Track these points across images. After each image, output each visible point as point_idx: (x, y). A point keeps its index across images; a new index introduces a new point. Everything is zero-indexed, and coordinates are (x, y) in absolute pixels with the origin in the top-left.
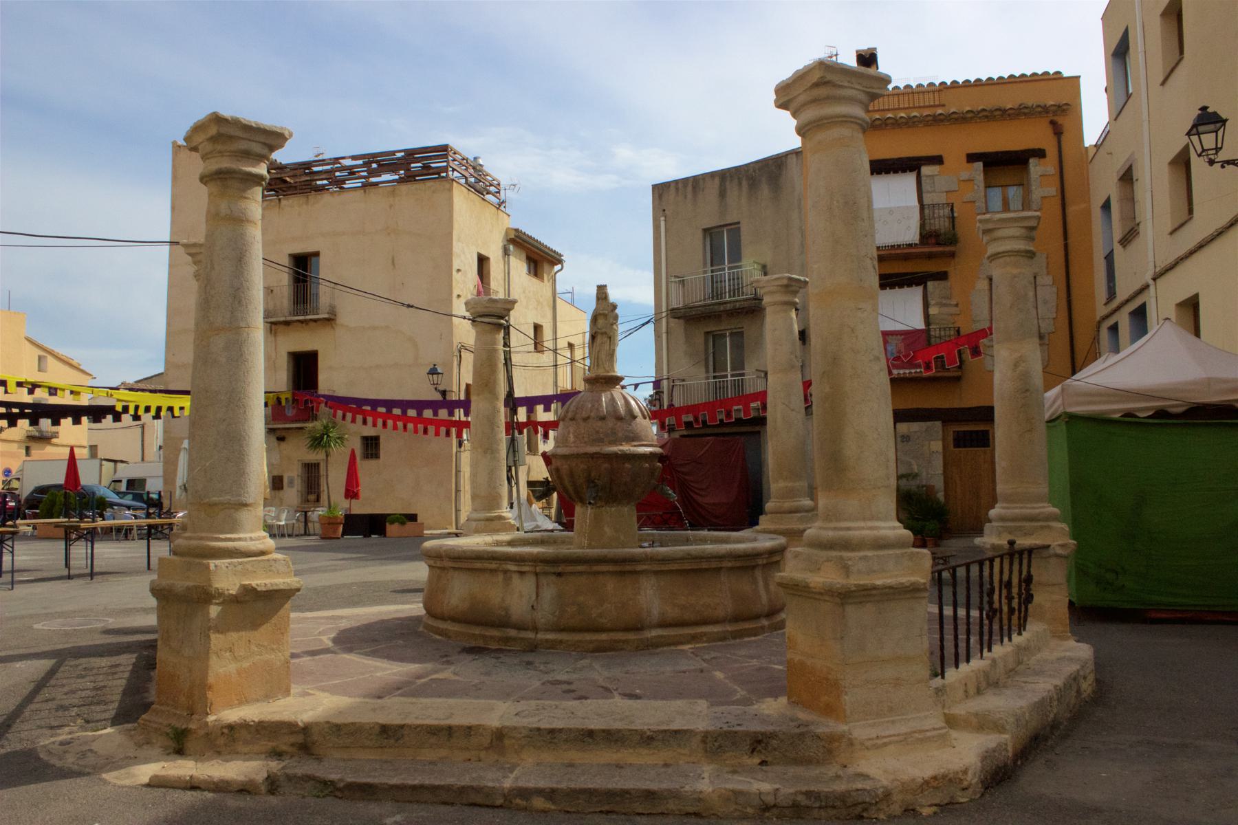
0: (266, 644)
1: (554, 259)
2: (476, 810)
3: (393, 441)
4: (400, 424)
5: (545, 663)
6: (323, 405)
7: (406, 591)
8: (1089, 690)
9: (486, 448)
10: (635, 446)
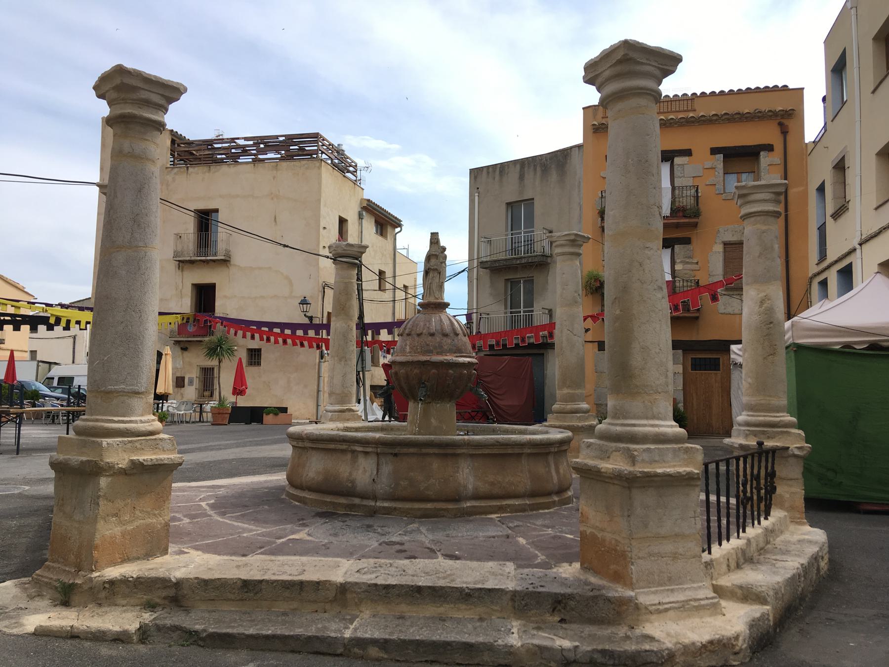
0: (149, 510)
1: (396, 223)
3: (271, 353)
4: (280, 340)
6: (219, 325)
8: (826, 568)
10: (457, 357)
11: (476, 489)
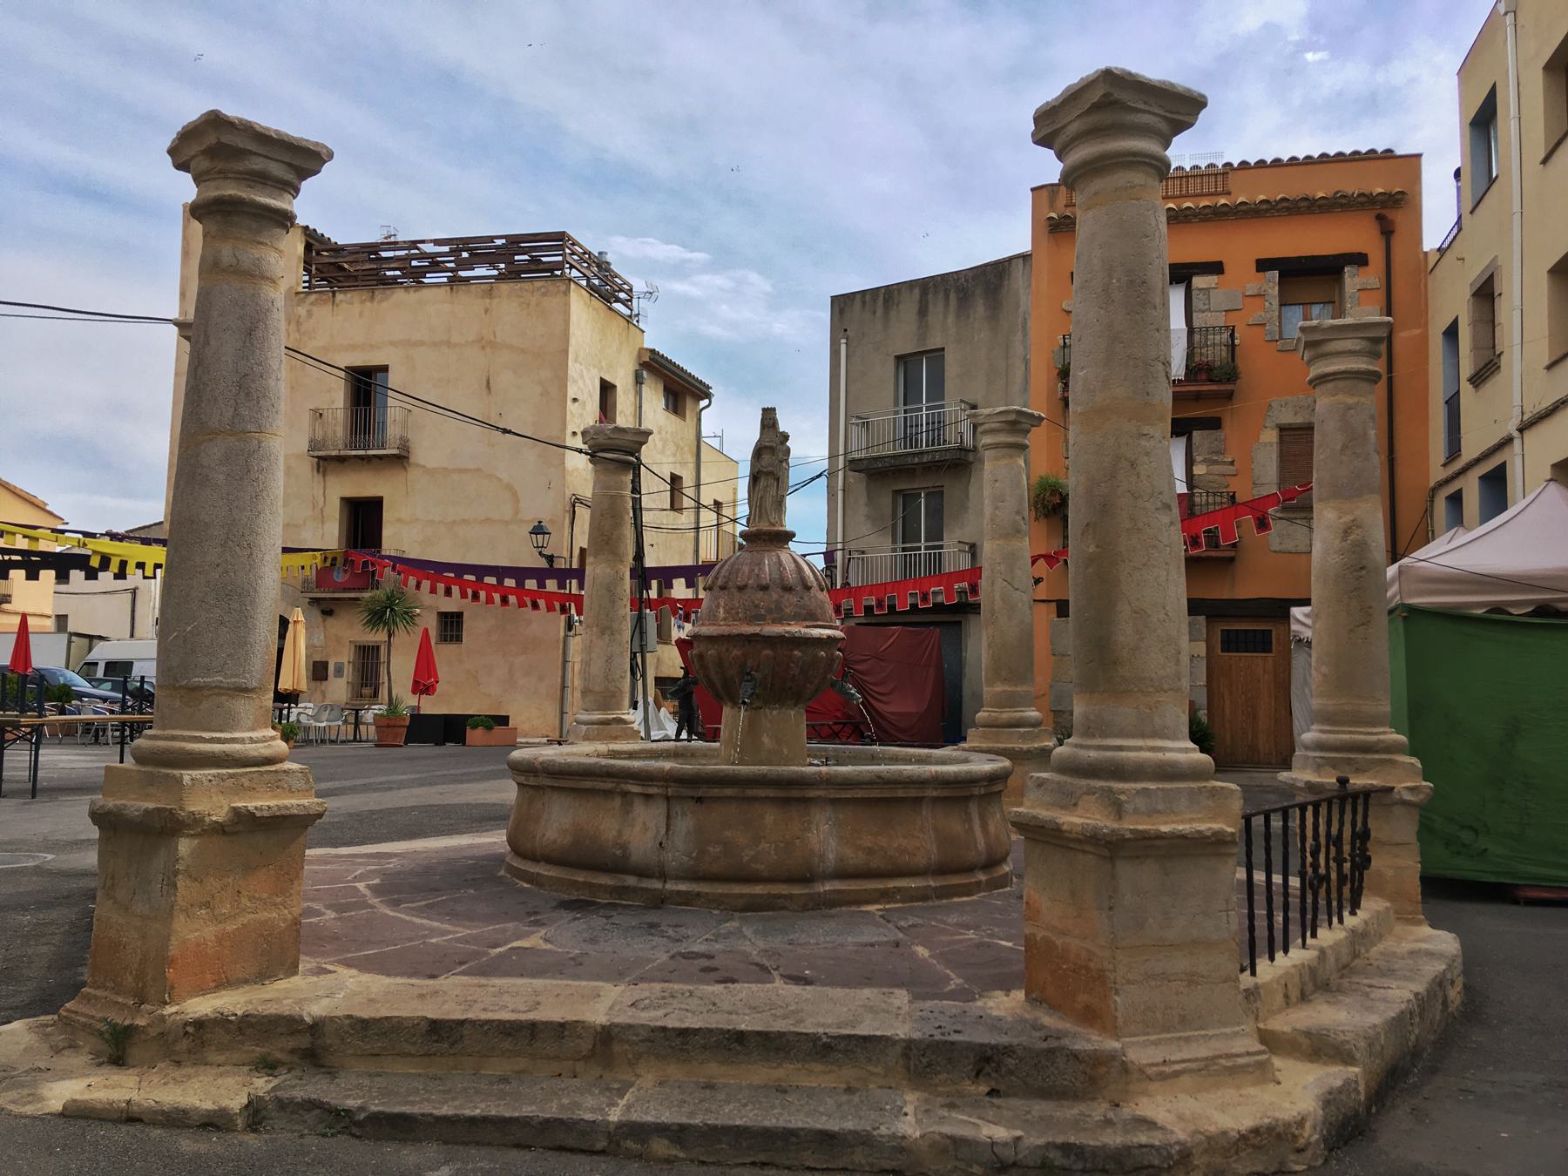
0: (265, 895)
1: (701, 392)
2: (565, 1157)
3: (479, 620)
4: (497, 597)
5: (676, 926)
6: (388, 570)
7: (482, 818)
8: (1458, 1001)
9: (606, 629)
10: (807, 627)
11: (841, 860)
